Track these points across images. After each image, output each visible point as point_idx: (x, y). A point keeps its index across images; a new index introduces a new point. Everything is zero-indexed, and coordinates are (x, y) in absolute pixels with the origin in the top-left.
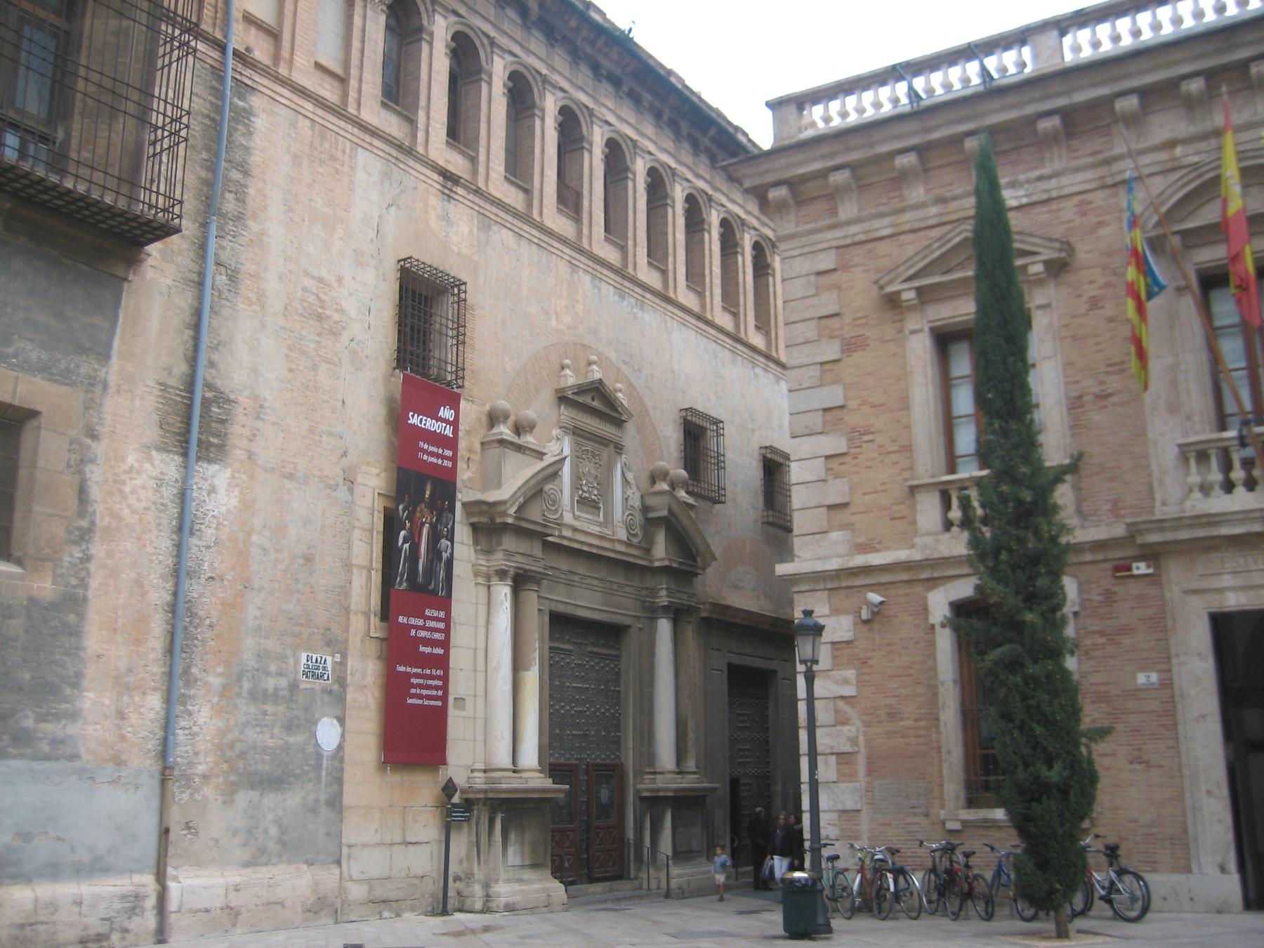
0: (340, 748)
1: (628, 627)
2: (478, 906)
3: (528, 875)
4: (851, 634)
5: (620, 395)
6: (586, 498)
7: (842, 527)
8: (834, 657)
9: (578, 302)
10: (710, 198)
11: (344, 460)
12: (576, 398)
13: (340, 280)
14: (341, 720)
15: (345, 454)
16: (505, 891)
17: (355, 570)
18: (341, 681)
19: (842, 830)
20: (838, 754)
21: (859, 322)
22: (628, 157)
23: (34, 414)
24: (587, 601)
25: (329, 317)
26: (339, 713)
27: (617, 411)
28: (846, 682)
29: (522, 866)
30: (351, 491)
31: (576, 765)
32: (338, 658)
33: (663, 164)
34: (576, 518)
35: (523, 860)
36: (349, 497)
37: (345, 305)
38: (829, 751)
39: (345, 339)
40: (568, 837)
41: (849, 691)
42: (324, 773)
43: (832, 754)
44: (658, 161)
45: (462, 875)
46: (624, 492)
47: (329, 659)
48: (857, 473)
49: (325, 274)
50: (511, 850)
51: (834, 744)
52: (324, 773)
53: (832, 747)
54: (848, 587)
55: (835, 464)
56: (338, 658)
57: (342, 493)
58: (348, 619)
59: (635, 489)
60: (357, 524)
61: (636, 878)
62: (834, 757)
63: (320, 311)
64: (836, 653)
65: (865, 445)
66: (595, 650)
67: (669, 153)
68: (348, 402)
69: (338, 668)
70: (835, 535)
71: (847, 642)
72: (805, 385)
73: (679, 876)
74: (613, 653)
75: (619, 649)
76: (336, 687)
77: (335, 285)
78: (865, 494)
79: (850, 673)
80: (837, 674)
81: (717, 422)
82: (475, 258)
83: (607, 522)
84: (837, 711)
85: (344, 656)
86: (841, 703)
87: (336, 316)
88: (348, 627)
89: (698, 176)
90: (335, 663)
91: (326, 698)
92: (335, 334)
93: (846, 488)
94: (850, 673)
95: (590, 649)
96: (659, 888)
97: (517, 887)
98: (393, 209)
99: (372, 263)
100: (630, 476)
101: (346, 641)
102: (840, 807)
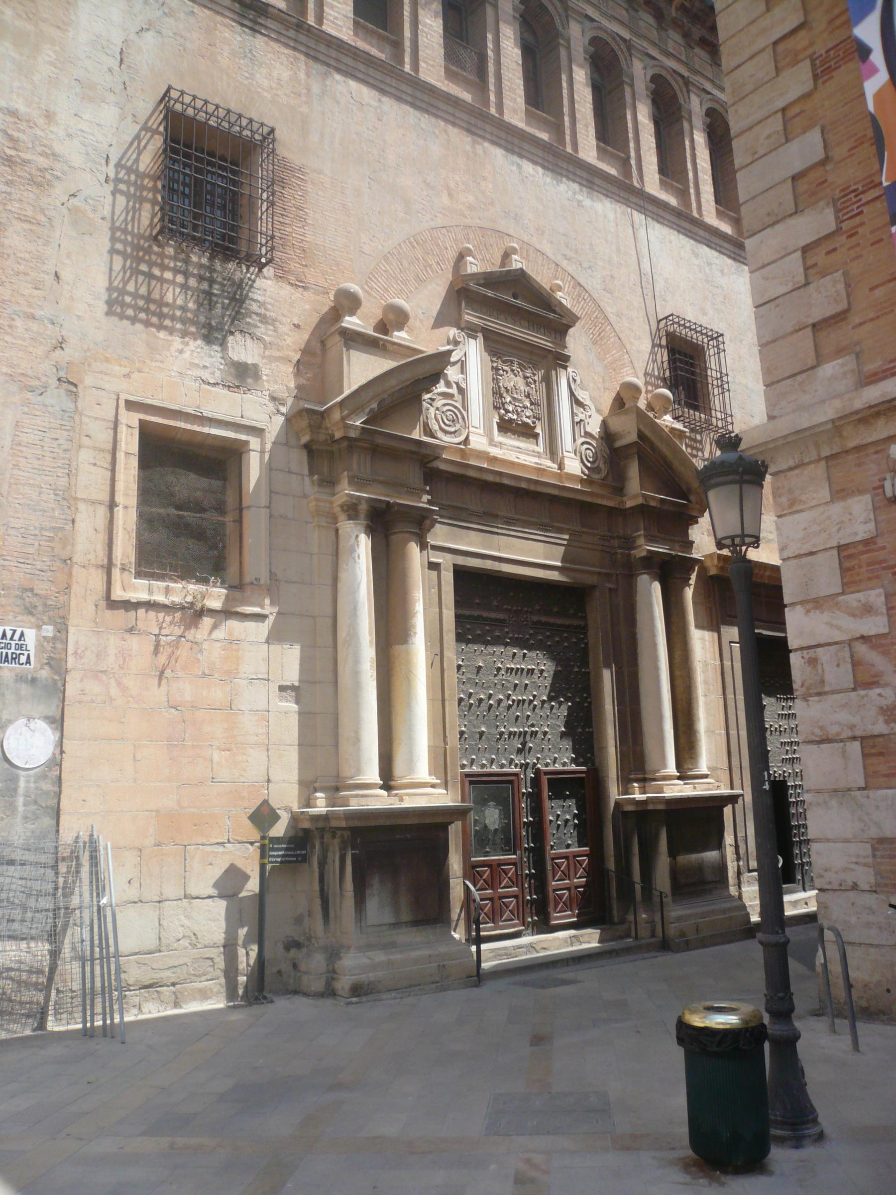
0: (56, 762)
1: (593, 587)
2: (318, 985)
3: (406, 936)
4: (871, 526)
5: (559, 294)
6: (511, 421)
7: (839, 352)
8: (844, 570)
9: (484, 179)
10: (687, 82)
11: (58, 352)
12: (483, 290)
13: (49, 116)
14: (58, 722)
15: (60, 345)
16: (354, 965)
17: (82, 506)
18: (57, 665)
19: (878, 873)
20: (863, 738)
21: (838, 22)
22: (558, 22)
23: (454, 565)
24: (531, 554)
25: (25, 162)
26: (54, 711)
27: (554, 312)
28: (868, 610)
29: (396, 925)
30: (74, 396)
31: (516, 775)
32: (49, 631)
33: (615, 36)
34: (491, 442)
35: (397, 912)
36: (71, 406)
37: (58, 148)
38: (847, 733)
39: (59, 192)
40: (506, 872)
41: (876, 625)
42: (20, 800)
43: (854, 738)
44: (605, 30)
45: (301, 939)
46: (573, 414)
47: (31, 636)
48: (859, 257)
49: (22, 108)
50: (373, 905)
51: (856, 720)
52: (20, 800)
53: (852, 727)
54: (858, 448)
55: (819, 257)
56: (49, 631)
57: (56, 398)
58: (70, 575)
59: (593, 411)
60: (85, 441)
61: (622, 921)
62: (857, 745)
63: (12, 152)
64: (847, 564)
65: (865, 209)
66: (544, 619)
67: (622, 23)
68: (64, 274)
69: (48, 646)
70: (829, 369)
71: (866, 542)
72: (761, 152)
73: (679, 919)
74: (575, 622)
75: (585, 618)
76: (45, 674)
77: (41, 121)
78: (872, 289)
79: (876, 596)
80: (853, 599)
81: (717, 337)
82: (304, 109)
83: (553, 451)
84: (856, 664)
85: (62, 628)
86: (862, 649)
87: (42, 162)
88: (69, 587)
89: (668, 54)
90: (41, 642)
91: (25, 689)
92: (39, 185)
93: (841, 287)
94: (876, 596)
95: (535, 618)
96: (653, 935)
97: (380, 957)
98: (149, 36)
99: (111, 98)
100: (581, 395)
101: (66, 606)
102: (874, 833)
